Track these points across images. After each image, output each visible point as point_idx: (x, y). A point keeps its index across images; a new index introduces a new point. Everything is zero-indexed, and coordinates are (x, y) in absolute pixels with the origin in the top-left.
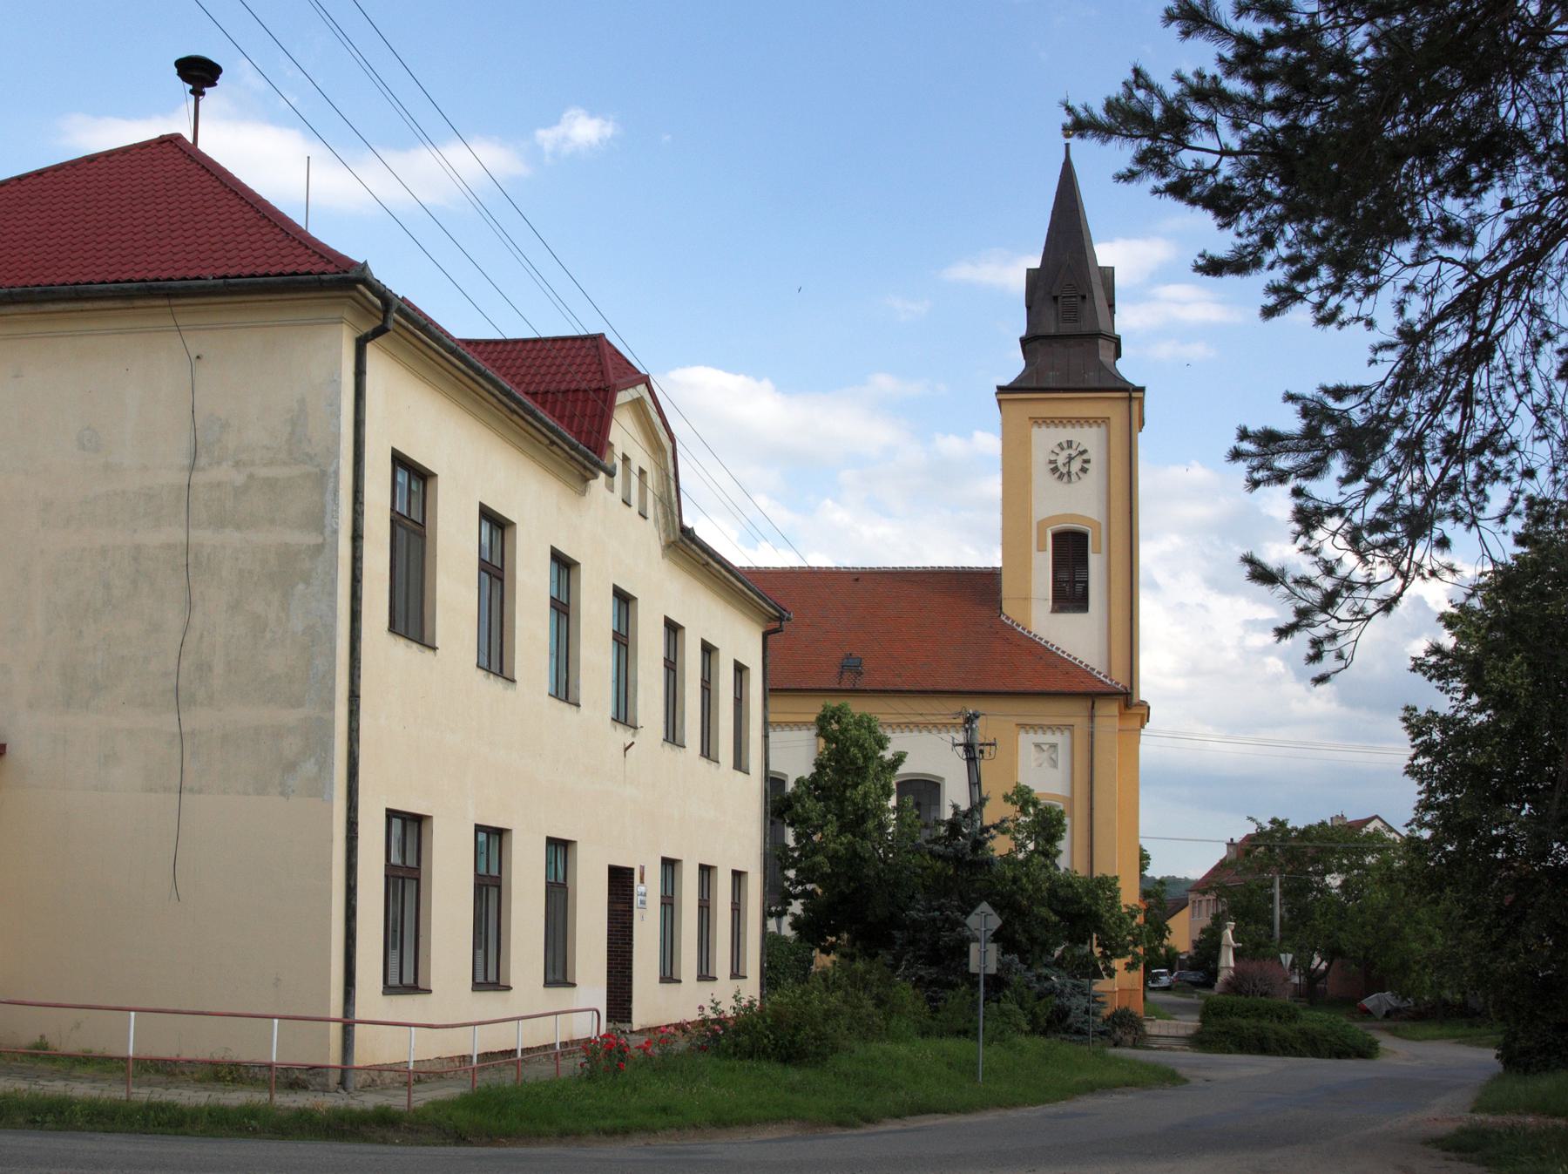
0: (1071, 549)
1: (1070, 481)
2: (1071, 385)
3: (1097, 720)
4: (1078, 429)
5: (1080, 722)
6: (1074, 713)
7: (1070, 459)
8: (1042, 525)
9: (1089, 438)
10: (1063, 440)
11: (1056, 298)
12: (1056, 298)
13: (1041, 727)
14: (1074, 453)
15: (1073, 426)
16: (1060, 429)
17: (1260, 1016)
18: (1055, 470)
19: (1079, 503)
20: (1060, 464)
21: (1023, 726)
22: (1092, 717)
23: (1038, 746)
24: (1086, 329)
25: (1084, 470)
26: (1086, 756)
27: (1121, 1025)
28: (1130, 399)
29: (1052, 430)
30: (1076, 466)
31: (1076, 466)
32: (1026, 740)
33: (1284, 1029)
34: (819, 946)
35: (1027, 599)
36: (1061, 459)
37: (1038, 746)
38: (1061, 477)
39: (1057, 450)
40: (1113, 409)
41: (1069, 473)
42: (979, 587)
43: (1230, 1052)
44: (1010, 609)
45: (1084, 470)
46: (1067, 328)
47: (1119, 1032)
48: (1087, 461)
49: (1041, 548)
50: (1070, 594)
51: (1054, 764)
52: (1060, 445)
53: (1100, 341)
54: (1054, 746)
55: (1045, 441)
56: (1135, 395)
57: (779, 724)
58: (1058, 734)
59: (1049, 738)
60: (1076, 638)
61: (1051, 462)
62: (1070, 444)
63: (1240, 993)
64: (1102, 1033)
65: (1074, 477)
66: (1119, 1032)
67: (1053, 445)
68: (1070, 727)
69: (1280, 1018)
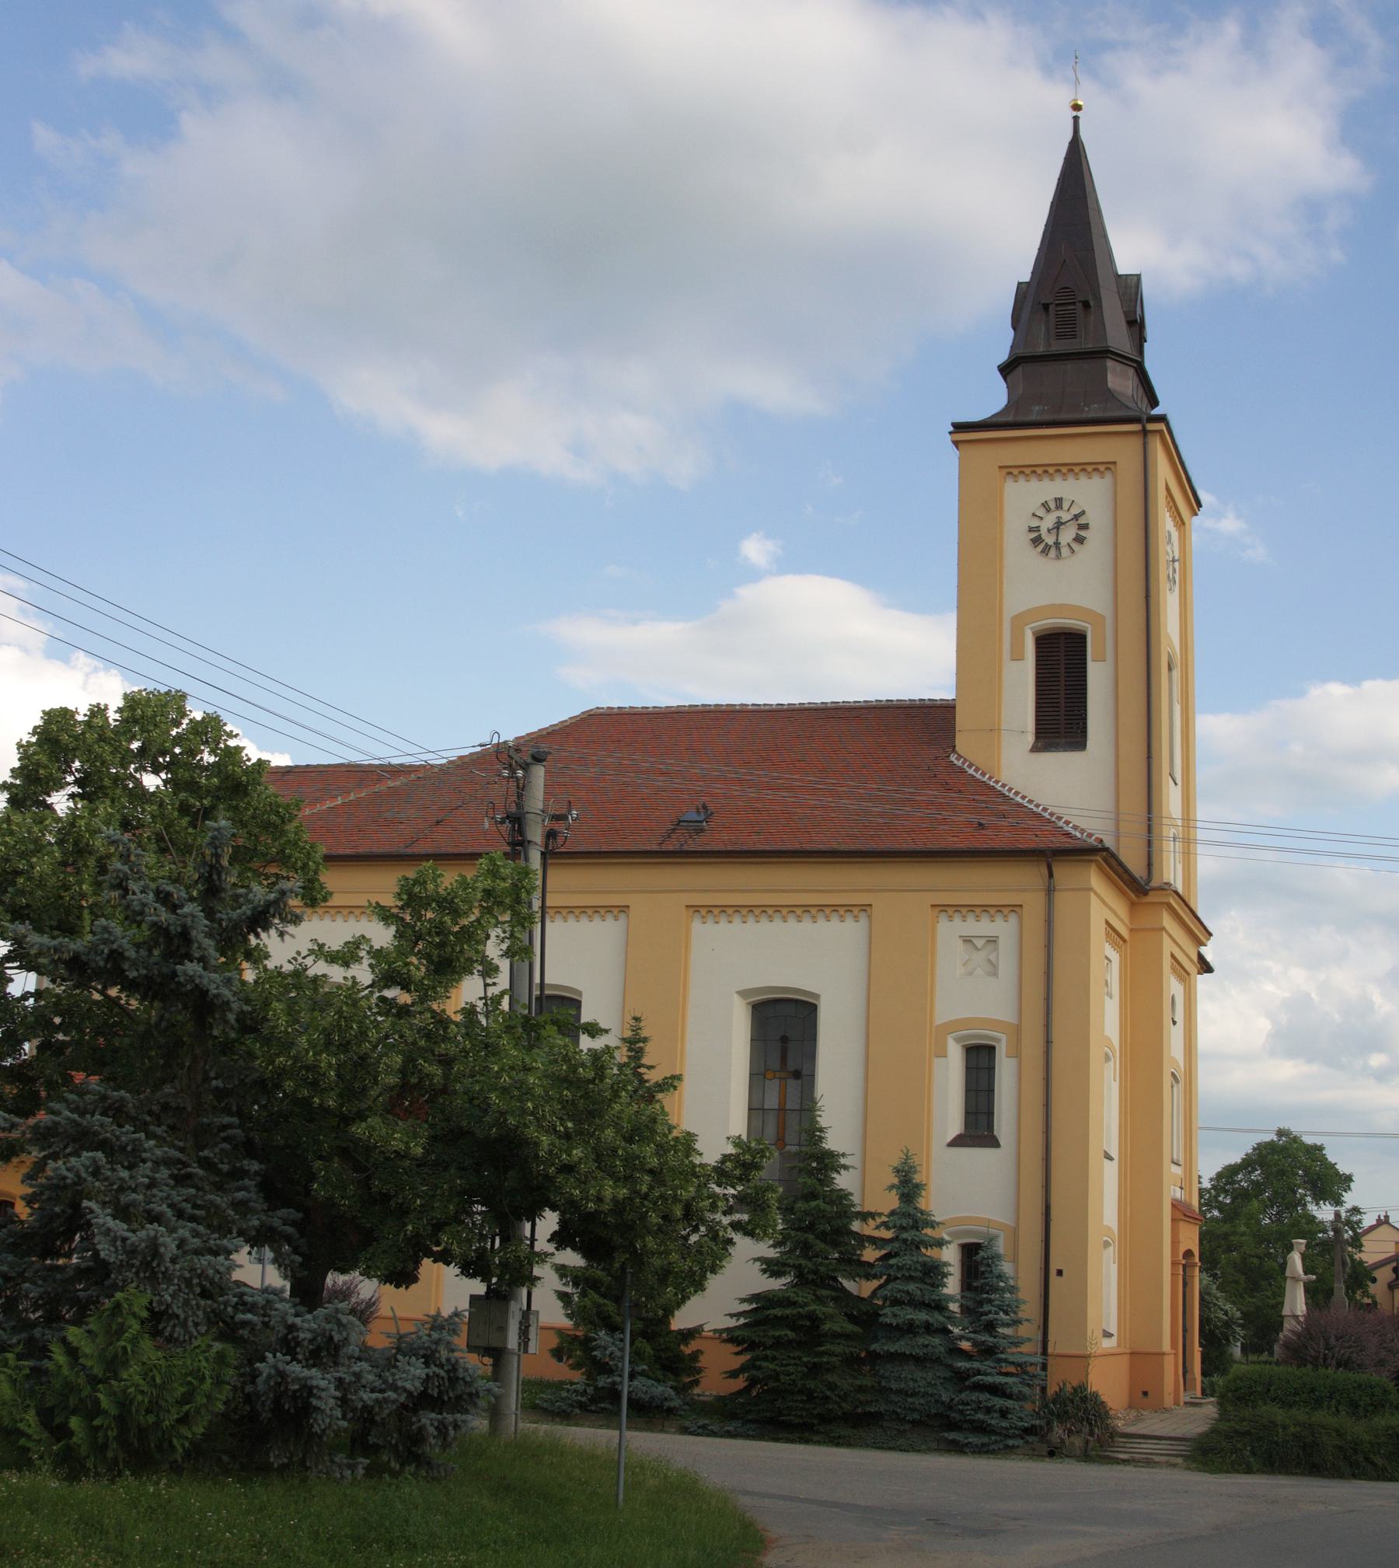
0: (1061, 657)
1: (1059, 556)
2: (1064, 416)
3: (1060, 898)
4: (1071, 479)
5: (1034, 902)
6: (1019, 883)
7: (1059, 525)
8: (1019, 621)
9: (1088, 495)
10: (1089, 518)
11: (1046, 307)
12: (1046, 307)
13: (971, 908)
14: (1066, 516)
15: (1064, 476)
16: (1046, 483)
17: (1318, 1403)
18: (1037, 541)
19: (1074, 587)
20: (1043, 531)
21: (942, 908)
22: (1050, 891)
23: (967, 940)
24: (1090, 346)
25: (1080, 540)
26: (1041, 956)
27: (1063, 1417)
28: (1145, 433)
29: (1034, 484)
30: (1067, 535)
31: (1067, 535)
32: (950, 931)
33: (1359, 1429)
34: (429, 1253)
35: (994, 730)
36: (1049, 521)
37: (967, 940)
38: (1046, 551)
39: (1041, 512)
40: (1121, 448)
41: (1057, 544)
42: (929, 722)
43: (1249, 1471)
44: (967, 746)
45: (1080, 540)
46: (1058, 347)
47: (1058, 1432)
48: (1085, 527)
49: (1017, 656)
50: (1061, 720)
51: (993, 969)
52: (1045, 505)
53: (1110, 363)
54: (992, 941)
55: (1023, 500)
56: (1150, 427)
57: (558, 910)
58: (999, 920)
59: (984, 927)
60: (1066, 788)
61: (1031, 530)
62: (1059, 502)
63: (1302, 1363)
64: (1029, 1431)
65: (1065, 551)
66: (1058, 1432)
67: (1035, 505)
68: (1015, 908)
69: (1354, 1405)
